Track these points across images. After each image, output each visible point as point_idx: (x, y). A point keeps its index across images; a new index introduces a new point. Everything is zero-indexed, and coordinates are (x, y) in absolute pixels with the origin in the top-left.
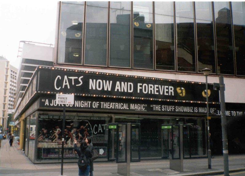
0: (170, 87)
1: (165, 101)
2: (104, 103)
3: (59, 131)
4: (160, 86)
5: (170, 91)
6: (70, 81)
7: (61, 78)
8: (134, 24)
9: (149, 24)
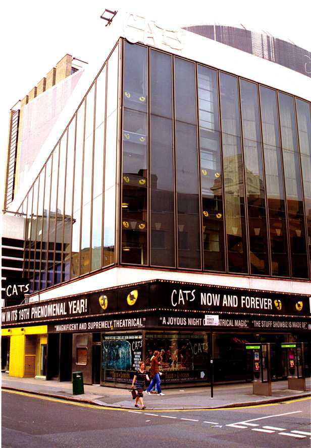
0: (269, 300)
1: (262, 314)
3: (163, 352)
5: (269, 304)
6: (184, 295)
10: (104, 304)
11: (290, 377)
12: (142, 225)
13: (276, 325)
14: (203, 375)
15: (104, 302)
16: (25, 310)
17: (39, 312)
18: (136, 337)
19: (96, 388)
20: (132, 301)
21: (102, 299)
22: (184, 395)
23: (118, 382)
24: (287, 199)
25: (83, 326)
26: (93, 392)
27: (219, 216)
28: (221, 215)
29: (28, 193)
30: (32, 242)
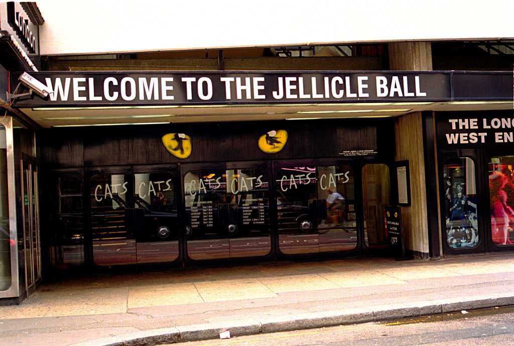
2: (239, 80)
7: (102, 187)
9: (272, 133)
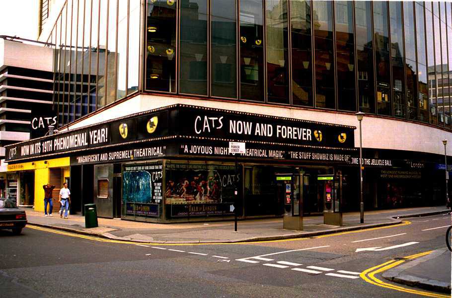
0: (308, 130)
3: (187, 183)
4: (298, 129)
5: (308, 135)
6: (210, 122)
8: (241, 40)
10: (124, 133)
11: (326, 211)
12: (169, 49)
13: (316, 157)
14: (232, 208)
15: (124, 131)
16: (48, 142)
17: (62, 143)
18: (157, 167)
19: (117, 222)
20: (152, 129)
21: (122, 128)
22: (205, 229)
23: (138, 216)
24: (336, 30)
25: (104, 157)
26: (107, 226)
27: (258, 42)
28: (260, 42)
29: (56, 22)
30: (60, 73)
